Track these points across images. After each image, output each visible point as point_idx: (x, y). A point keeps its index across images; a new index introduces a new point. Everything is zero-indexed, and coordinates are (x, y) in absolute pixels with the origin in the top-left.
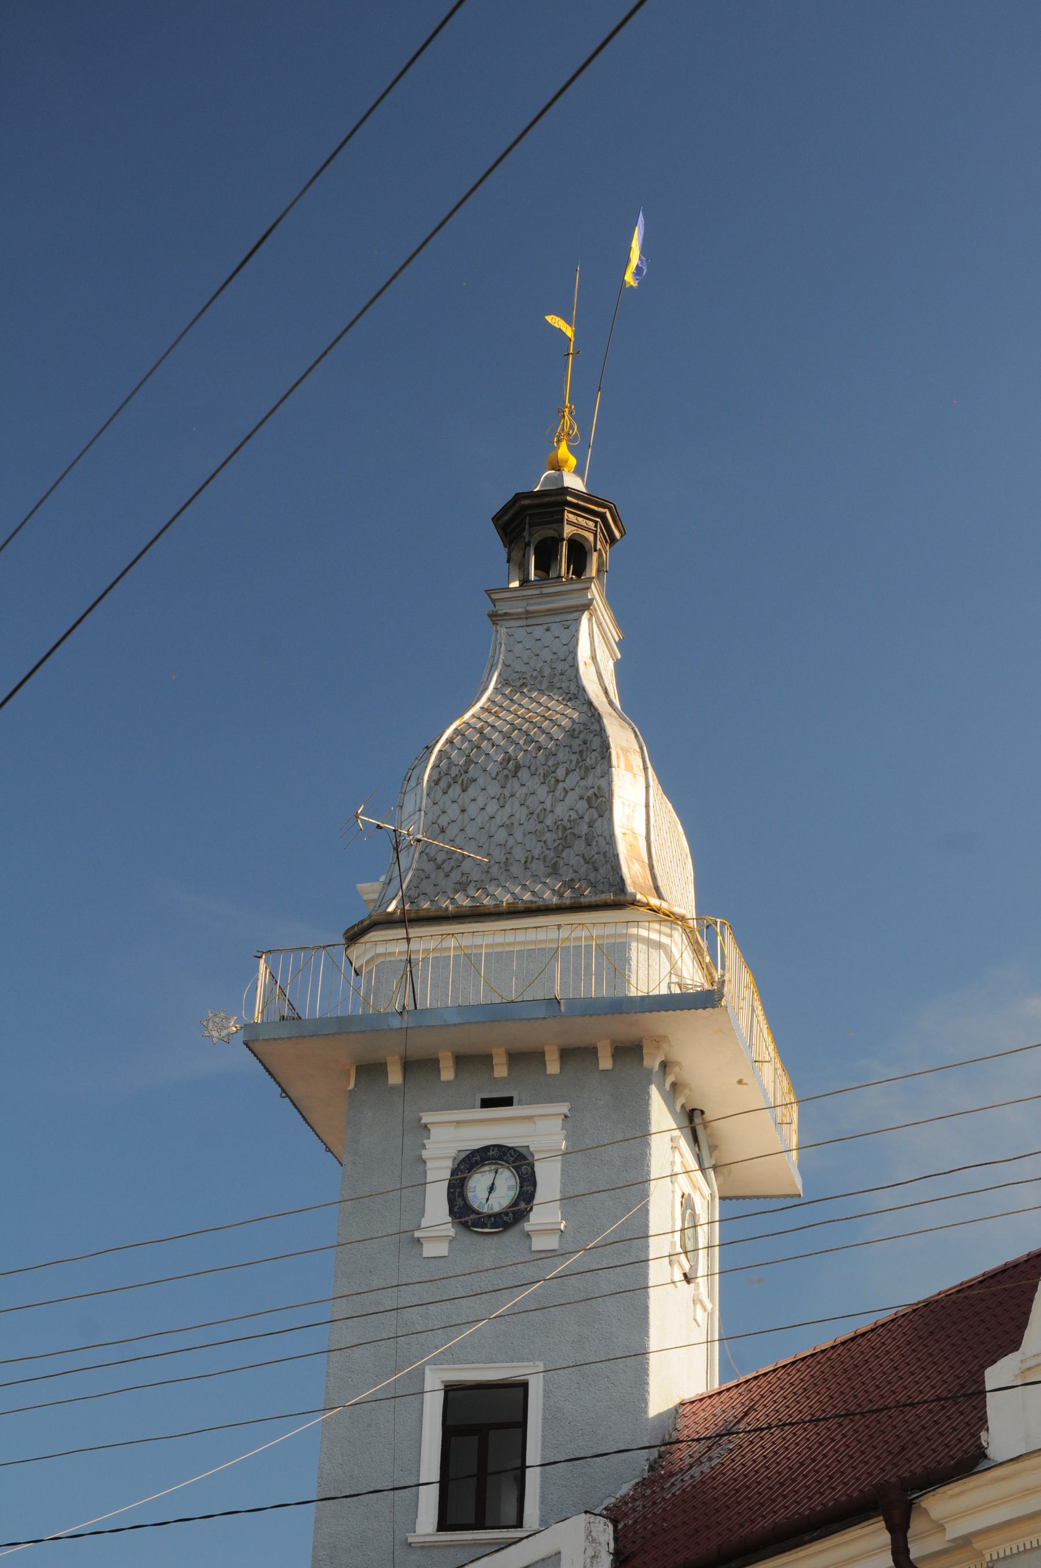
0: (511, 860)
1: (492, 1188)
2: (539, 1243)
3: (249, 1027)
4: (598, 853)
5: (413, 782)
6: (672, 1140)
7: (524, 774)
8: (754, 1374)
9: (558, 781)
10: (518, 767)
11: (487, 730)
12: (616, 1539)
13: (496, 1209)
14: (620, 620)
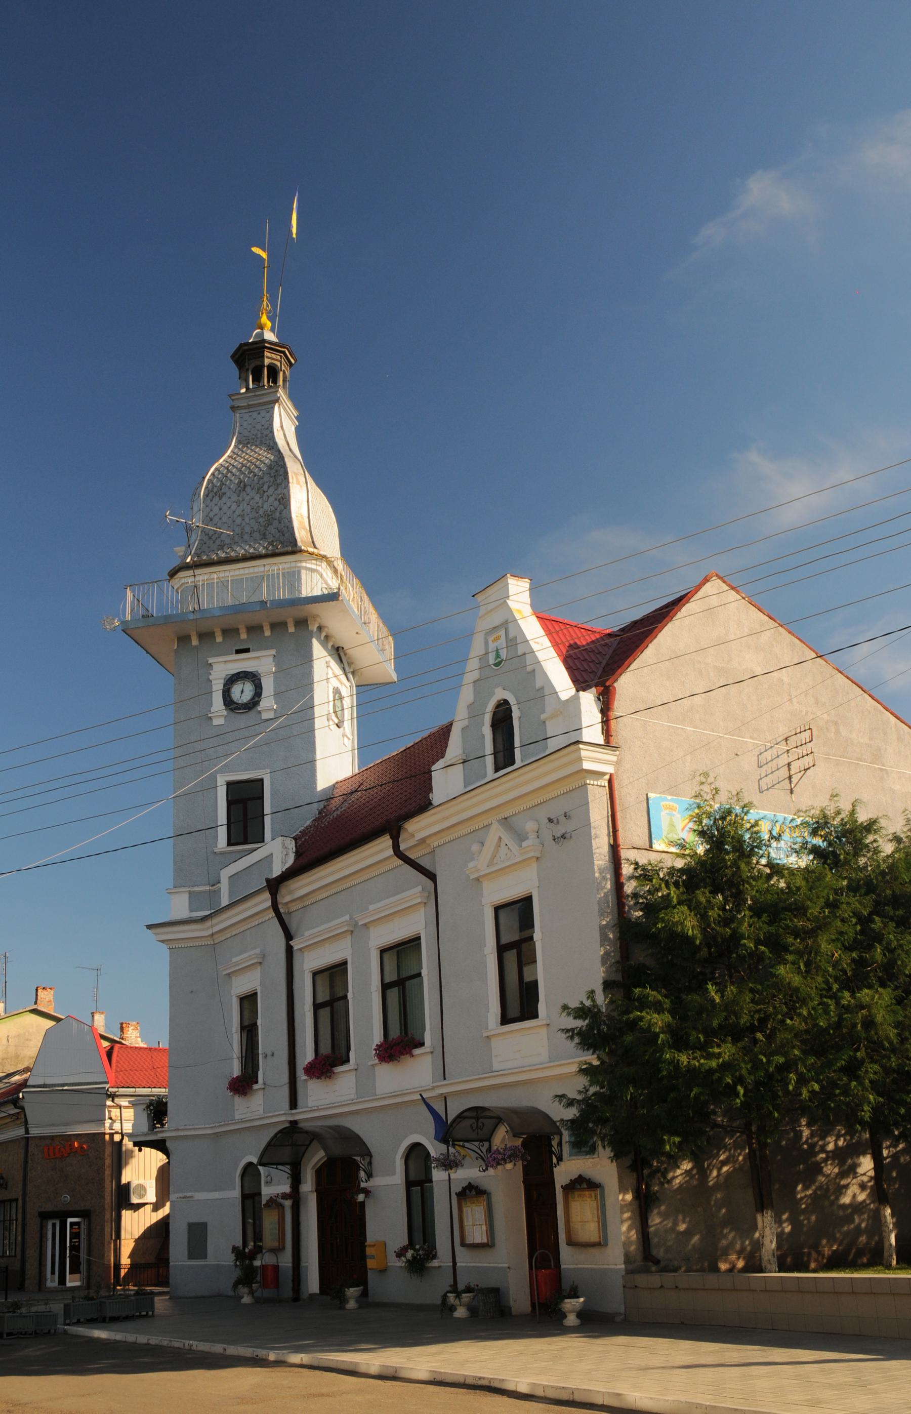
0: (244, 533)
1: (242, 692)
2: (265, 716)
3: (123, 623)
4: (284, 527)
5: (197, 495)
6: (326, 663)
7: (248, 489)
8: (366, 768)
9: (264, 492)
10: (245, 486)
11: (230, 467)
12: (296, 846)
13: (245, 701)
14: (296, 406)
